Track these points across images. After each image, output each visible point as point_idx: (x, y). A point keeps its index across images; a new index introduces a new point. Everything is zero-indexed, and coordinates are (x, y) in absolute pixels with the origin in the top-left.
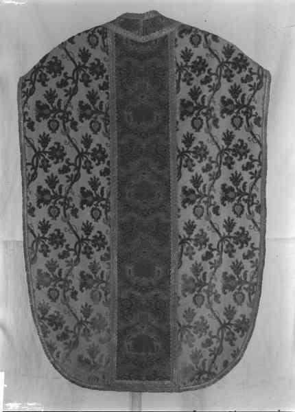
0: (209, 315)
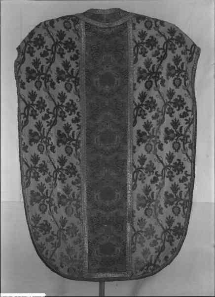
0: (156, 224)
